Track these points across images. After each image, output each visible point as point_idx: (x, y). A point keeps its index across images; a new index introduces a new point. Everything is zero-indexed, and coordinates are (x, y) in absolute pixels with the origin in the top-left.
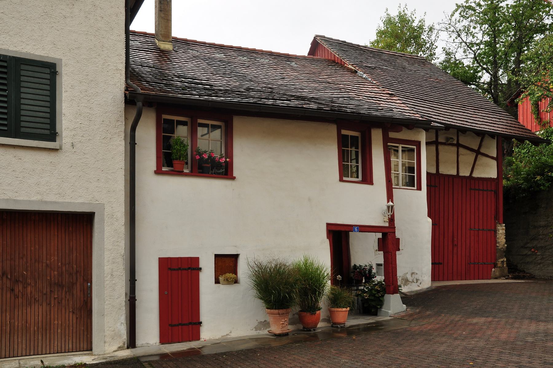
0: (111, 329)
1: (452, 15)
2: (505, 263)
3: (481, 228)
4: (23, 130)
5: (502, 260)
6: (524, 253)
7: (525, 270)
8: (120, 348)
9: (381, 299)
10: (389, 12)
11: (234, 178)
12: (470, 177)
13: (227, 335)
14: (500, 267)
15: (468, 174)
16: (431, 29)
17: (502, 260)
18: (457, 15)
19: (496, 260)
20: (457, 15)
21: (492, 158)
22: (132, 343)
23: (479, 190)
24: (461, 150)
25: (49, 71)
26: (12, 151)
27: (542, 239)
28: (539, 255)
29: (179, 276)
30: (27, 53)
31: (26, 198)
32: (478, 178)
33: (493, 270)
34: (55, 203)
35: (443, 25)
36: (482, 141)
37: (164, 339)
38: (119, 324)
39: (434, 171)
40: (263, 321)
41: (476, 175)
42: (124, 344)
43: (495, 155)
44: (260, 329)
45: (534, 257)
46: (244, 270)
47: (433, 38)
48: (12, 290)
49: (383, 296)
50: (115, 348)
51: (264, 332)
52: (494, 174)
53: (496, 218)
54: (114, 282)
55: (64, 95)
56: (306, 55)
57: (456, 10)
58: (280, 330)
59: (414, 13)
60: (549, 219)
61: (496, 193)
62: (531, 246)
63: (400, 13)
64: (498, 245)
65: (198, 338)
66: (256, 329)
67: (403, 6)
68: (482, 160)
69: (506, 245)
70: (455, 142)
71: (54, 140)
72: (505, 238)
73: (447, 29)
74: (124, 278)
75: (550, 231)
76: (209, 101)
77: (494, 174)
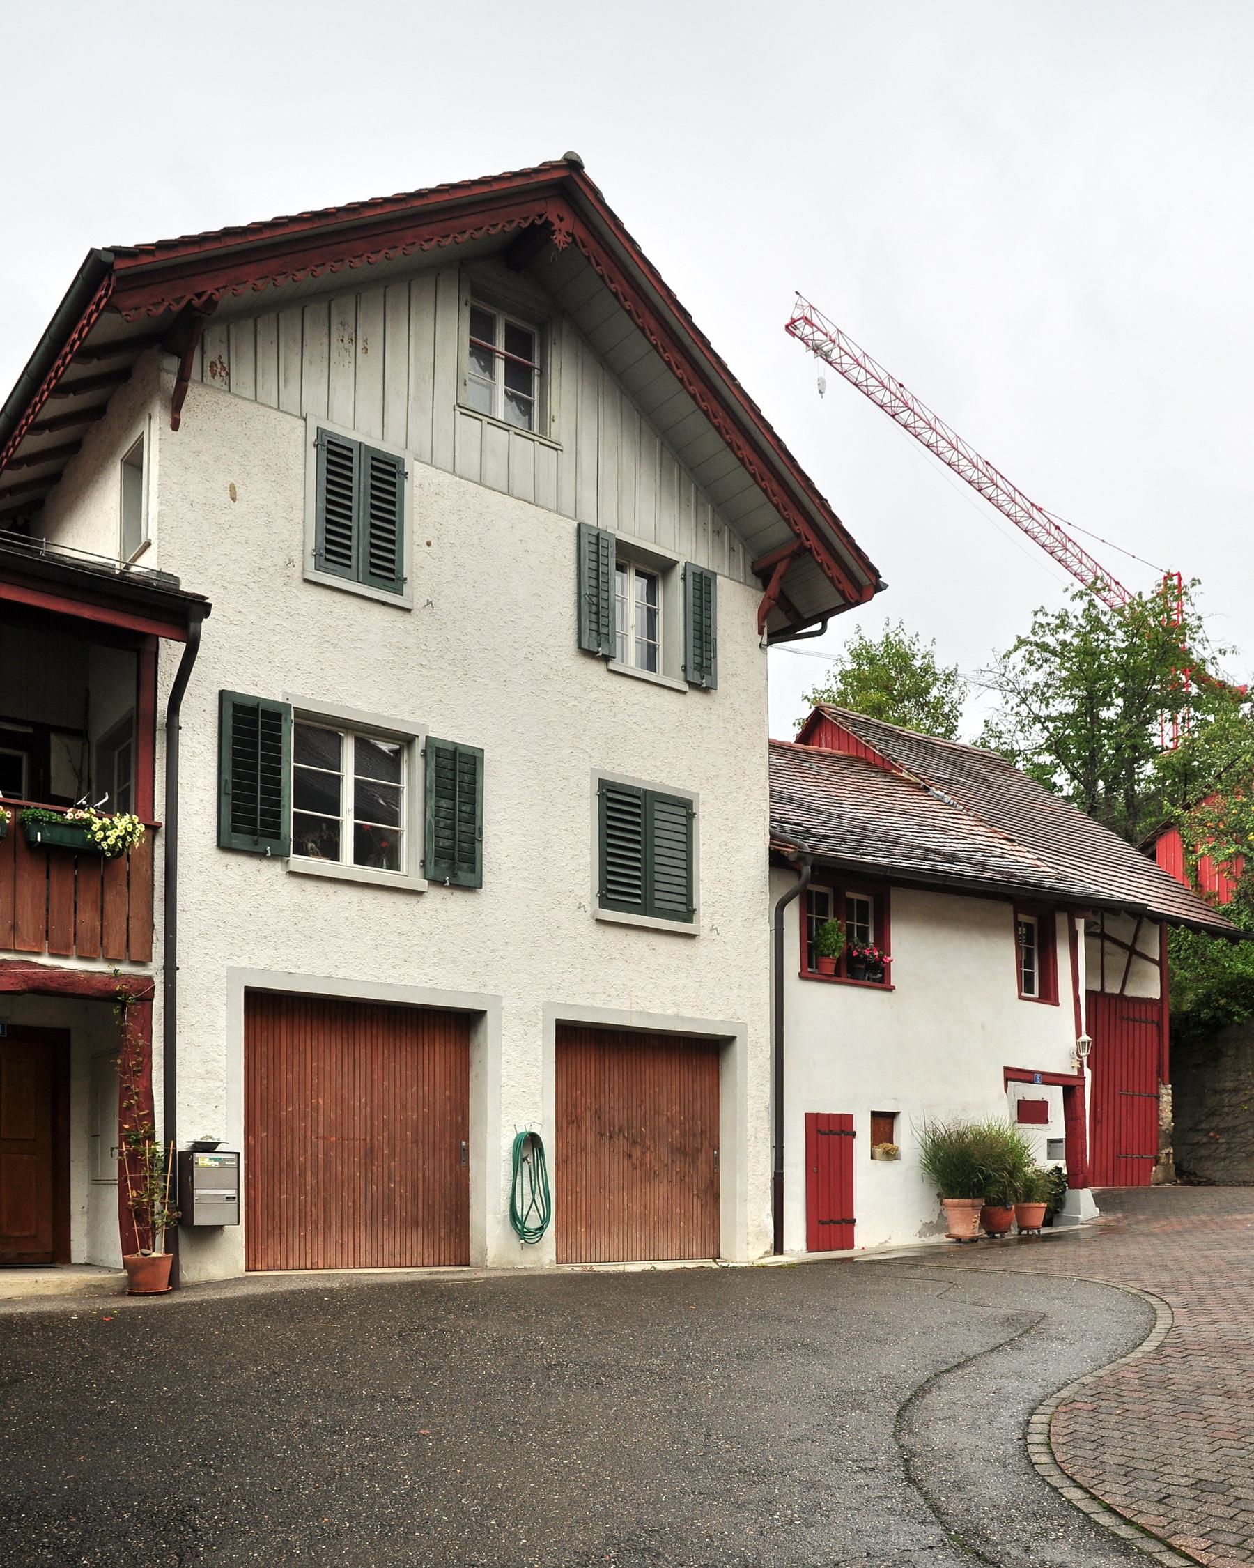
1: (1007, 655)
4: (658, 904)
5: (1167, 1151)
10: (862, 633)
11: (891, 989)
12: (1121, 997)
15: (1117, 991)
17: (1167, 1151)
19: (1158, 1150)
20: (1018, 659)
21: (1153, 961)
22: (778, 1248)
24: (1107, 944)
25: (685, 807)
26: (633, 935)
27: (1228, 1114)
29: (829, 1135)
30: (662, 784)
31: (661, 1012)
34: (693, 1020)
36: (1137, 930)
37: (812, 1245)
39: (1097, 987)
41: (1129, 992)
46: (907, 1138)
47: (955, 694)
48: (630, 1156)
49: (1063, 1192)
51: (940, 1239)
52: (1155, 993)
53: (1160, 1074)
55: (702, 849)
56: (792, 740)
57: (1016, 649)
60: (1242, 1077)
63: (887, 637)
65: (851, 1246)
66: (921, 1234)
67: (894, 625)
71: (690, 921)
75: (1244, 1099)
77: (1155, 993)
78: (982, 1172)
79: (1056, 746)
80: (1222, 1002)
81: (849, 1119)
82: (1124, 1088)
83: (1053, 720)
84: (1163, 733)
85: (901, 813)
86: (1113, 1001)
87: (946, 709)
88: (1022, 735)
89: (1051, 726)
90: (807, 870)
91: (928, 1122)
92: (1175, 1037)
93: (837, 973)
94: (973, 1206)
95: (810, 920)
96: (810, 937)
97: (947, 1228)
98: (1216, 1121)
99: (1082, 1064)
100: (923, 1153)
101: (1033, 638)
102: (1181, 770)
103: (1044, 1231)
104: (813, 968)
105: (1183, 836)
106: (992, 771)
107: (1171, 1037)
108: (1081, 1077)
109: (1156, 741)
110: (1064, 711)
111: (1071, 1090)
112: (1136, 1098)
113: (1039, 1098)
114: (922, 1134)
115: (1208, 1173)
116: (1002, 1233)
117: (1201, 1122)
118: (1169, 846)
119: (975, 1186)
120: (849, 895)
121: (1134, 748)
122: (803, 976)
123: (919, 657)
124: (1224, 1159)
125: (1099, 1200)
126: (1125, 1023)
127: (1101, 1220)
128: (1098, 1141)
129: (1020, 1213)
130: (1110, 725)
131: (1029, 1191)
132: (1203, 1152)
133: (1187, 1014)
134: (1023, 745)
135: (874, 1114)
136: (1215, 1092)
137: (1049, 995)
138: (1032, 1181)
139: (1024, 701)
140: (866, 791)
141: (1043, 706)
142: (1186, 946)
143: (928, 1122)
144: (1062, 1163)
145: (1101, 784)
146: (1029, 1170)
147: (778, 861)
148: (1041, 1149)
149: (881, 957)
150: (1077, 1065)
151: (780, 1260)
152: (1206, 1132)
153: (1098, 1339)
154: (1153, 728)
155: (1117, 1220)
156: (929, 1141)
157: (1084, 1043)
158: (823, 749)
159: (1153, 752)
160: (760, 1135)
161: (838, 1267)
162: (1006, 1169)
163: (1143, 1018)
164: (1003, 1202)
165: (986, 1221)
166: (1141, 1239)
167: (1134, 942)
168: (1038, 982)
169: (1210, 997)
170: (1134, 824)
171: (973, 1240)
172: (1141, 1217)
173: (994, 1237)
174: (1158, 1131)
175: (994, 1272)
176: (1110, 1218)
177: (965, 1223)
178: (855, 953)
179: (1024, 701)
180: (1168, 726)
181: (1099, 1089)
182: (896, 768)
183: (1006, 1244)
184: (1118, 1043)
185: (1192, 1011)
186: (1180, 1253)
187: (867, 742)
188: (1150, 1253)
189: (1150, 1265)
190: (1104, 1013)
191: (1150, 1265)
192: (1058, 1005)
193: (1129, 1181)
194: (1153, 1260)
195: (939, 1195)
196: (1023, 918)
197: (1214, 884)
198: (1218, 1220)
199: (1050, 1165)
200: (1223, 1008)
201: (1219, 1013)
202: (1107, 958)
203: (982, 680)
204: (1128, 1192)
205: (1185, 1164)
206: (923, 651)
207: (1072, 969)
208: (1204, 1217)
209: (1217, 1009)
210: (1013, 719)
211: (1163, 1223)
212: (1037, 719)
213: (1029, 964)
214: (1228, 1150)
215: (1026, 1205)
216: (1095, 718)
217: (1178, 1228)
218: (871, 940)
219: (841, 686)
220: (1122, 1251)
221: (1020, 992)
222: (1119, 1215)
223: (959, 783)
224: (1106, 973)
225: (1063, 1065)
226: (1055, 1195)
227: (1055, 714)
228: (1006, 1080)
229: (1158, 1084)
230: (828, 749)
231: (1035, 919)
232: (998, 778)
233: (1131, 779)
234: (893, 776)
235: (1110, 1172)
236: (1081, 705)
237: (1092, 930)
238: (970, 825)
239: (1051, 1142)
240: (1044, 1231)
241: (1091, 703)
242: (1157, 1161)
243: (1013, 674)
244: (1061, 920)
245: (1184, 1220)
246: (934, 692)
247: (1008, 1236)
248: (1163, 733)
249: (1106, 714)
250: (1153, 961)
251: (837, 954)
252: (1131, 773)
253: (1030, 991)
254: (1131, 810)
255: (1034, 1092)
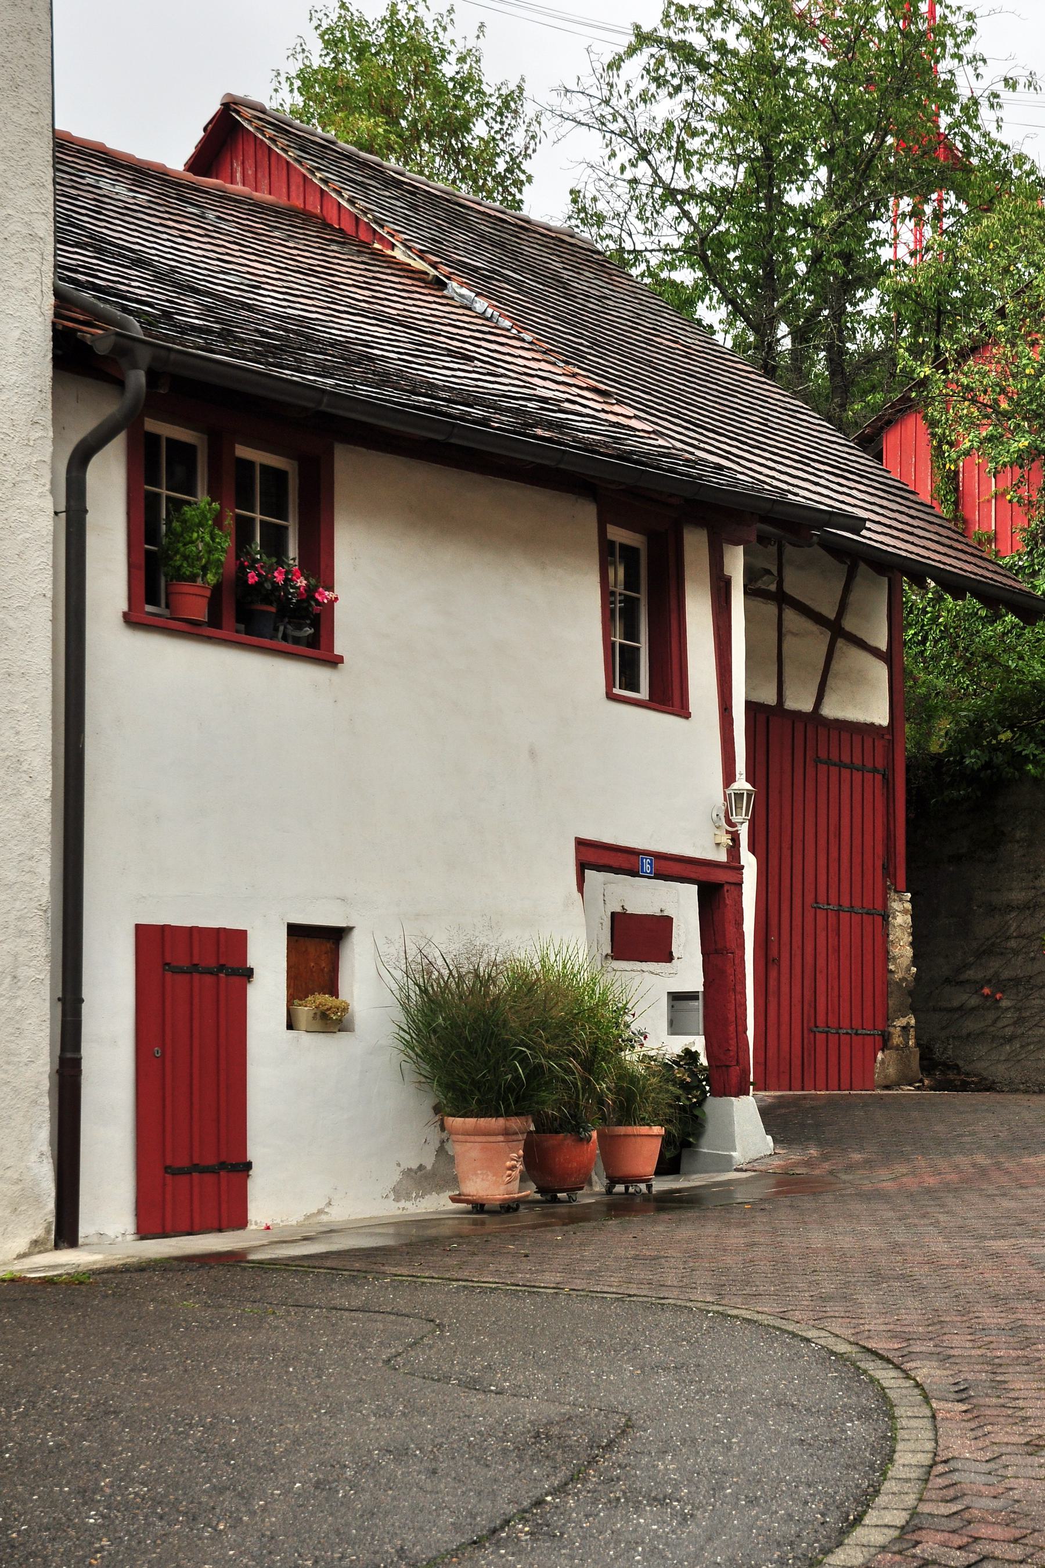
0: (9, 1173)
1: (615, 65)
2: (912, 1032)
3: (845, 902)
5: (902, 1022)
6: (956, 1004)
7: (961, 1063)
8: (37, 1246)
9: (697, 1112)
11: (334, 662)
12: (815, 717)
13: (320, 1212)
14: (897, 1048)
15: (807, 707)
16: (510, 104)
17: (902, 1022)
18: (634, 68)
19: (888, 1019)
20: (634, 68)
21: (875, 652)
22: (66, 1230)
23: (840, 765)
24: (791, 616)
27: (1016, 952)
28: (1008, 1009)
29: (191, 980)
32: (837, 721)
33: (880, 1056)
35: (584, 103)
37: (150, 1221)
38: (34, 1157)
39: (768, 697)
40: (415, 1166)
41: (831, 710)
42: (48, 1232)
43: (884, 647)
44: (408, 1198)
45: (991, 1016)
46: (367, 984)
47: (519, 138)
49: (701, 1103)
50: (21, 1244)
51: (437, 1204)
52: (880, 716)
53: (888, 871)
54: (19, 1003)
57: (632, 51)
58: (503, 1188)
59: (446, 21)
61: (888, 782)
62: (980, 975)
64: (892, 967)
65: (240, 1221)
66: (398, 1193)
68: (854, 658)
69: (914, 970)
70: (773, 588)
72: (912, 944)
73: (602, 121)
74: (45, 991)
76: (324, 391)
77: (880, 716)
78: (524, 1060)
79: (703, 250)
80: (1005, 736)
81: (239, 938)
82: (822, 897)
83: (701, 198)
84: (898, 238)
85: (382, 319)
86: (799, 727)
87: (501, 166)
88: (640, 226)
89: (694, 210)
90: (137, 378)
91: (412, 951)
92: (916, 801)
93: (215, 620)
94: (506, 1133)
95: (152, 502)
96: (151, 534)
97: (454, 1181)
98: (994, 965)
99: (735, 838)
100: (401, 1017)
101: (663, 32)
102: (932, 304)
103: (661, 1185)
104: (158, 598)
105: (933, 423)
106: (576, 269)
107: (908, 802)
108: (734, 866)
109: (886, 253)
110: (720, 184)
111: (715, 891)
112: (844, 917)
113: (652, 910)
114: (398, 974)
115: (980, 1066)
116: (572, 1190)
117: (966, 966)
118: (908, 446)
119: (509, 1089)
120: (243, 452)
121: (847, 258)
122: (133, 620)
123: (452, 58)
124: (1010, 1040)
125: (772, 1118)
126: (823, 768)
127: (777, 1162)
128: (773, 1001)
129: (610, 1146)
130: (805, 218)
131: (628, 1103)
132: (971, 1025)
133: (937, 758)
134: (641, 242)
135: (296, 932)
136: (992, 910)
137: (669, 696)
138: (633, 1079)
139: (644, 155)
140: (312, 272)
141: (680, 167)
142: (935, 633)
143: (412, 951)
144: (698, 1044)
145: (783, 329)
146: (629, 1056)
147: (77, 354)
148: (654, 1015)
149: (311, 590)
150: (726, 840)
151: (68, 1259)
152: (977, 986)
153: (752, 1501)
154: (881, 228)
155: (808, 1163)
156: (414, 992)
157: (739, 796)
158: (239, 188)
159: (876, 273)
160: (23, 972)
161: (189, 1277)
162: (576, 1055)
163: (857, 761)
164: (573, 1125)
165: (536, 1163)
166: (858, 1207)
167: (843, 607)
168: (646, 668)
169: (981, 726)
170: (843, 407)
171: (509, 1208)
172: (857, 1157)
173: (555, 1200)
174: (887, 983)
175: (532, 1291)
176: (795, 1157)
177: (491, 1170)
178: (252, 578)
179: (644, 155)
180: (906, 230)
181: (773, 897)
182: (382, 239)
183: (578, 1217)
184: (810, 794)
185: (949, 753)
186: (940, 1246)
187: (325, 181)
188: (877, 1243)
189: (877, 1276)
190: (781, 745)
191: (877, 1276)
192: (687, 716)
193: (833, 1081)
194: (883, 1261)
195: (437, 1109)
196: (618, 535)
197: (987, 519)
198: (1009, 1165)
199: (675, 1046)
200: (1005, 748)
201: (999, 758)
202: (788, 643)
203: (568, 109)
204: (831, 1101)
205: (938, 1048)
206: (460, 47)
207: (716, 639)
208: (981, 1159)
209: (995, 749)
210: (623, 188)
211: (901, 1169)
212: (670, 194)
213: (631, 633)
214: (1019, 1021)
215: (622, 1130)
216: (775, 201)
217: (931, 1181)
218: (293, 551)
219: (299, 100)
220: (818, 1238)
221: (610, 684)
222: (813, 1152)
223: (508, 280)
224: (787, 670)
225: (704, 845)
226: (682, 1105)
227: (702, 187)
228: (582, 868)
229: (886, 890)
230: (246, 190)
231: (646, 530)
232: (585, 282)
233: (841, 332)
234: (375, 254)
235: (797, 1062)
236: (751, 173)
237: (760, 584)
238: (525, 359)
239: (676, 997)
240: (661, 1185)
241: (769, 172)
242: (885, 1042)
243: (625, 101)
244: (695, 546)
245: (943, 1164)
246: (480, 128)
247: (585, 1198)
248: (898, 238)
249: (798, 196)
250: (875, 652)
251: (210, 577)
252: (839, 314)
253: (635, 687)
254: (838, 379)
255: (646, 897)
